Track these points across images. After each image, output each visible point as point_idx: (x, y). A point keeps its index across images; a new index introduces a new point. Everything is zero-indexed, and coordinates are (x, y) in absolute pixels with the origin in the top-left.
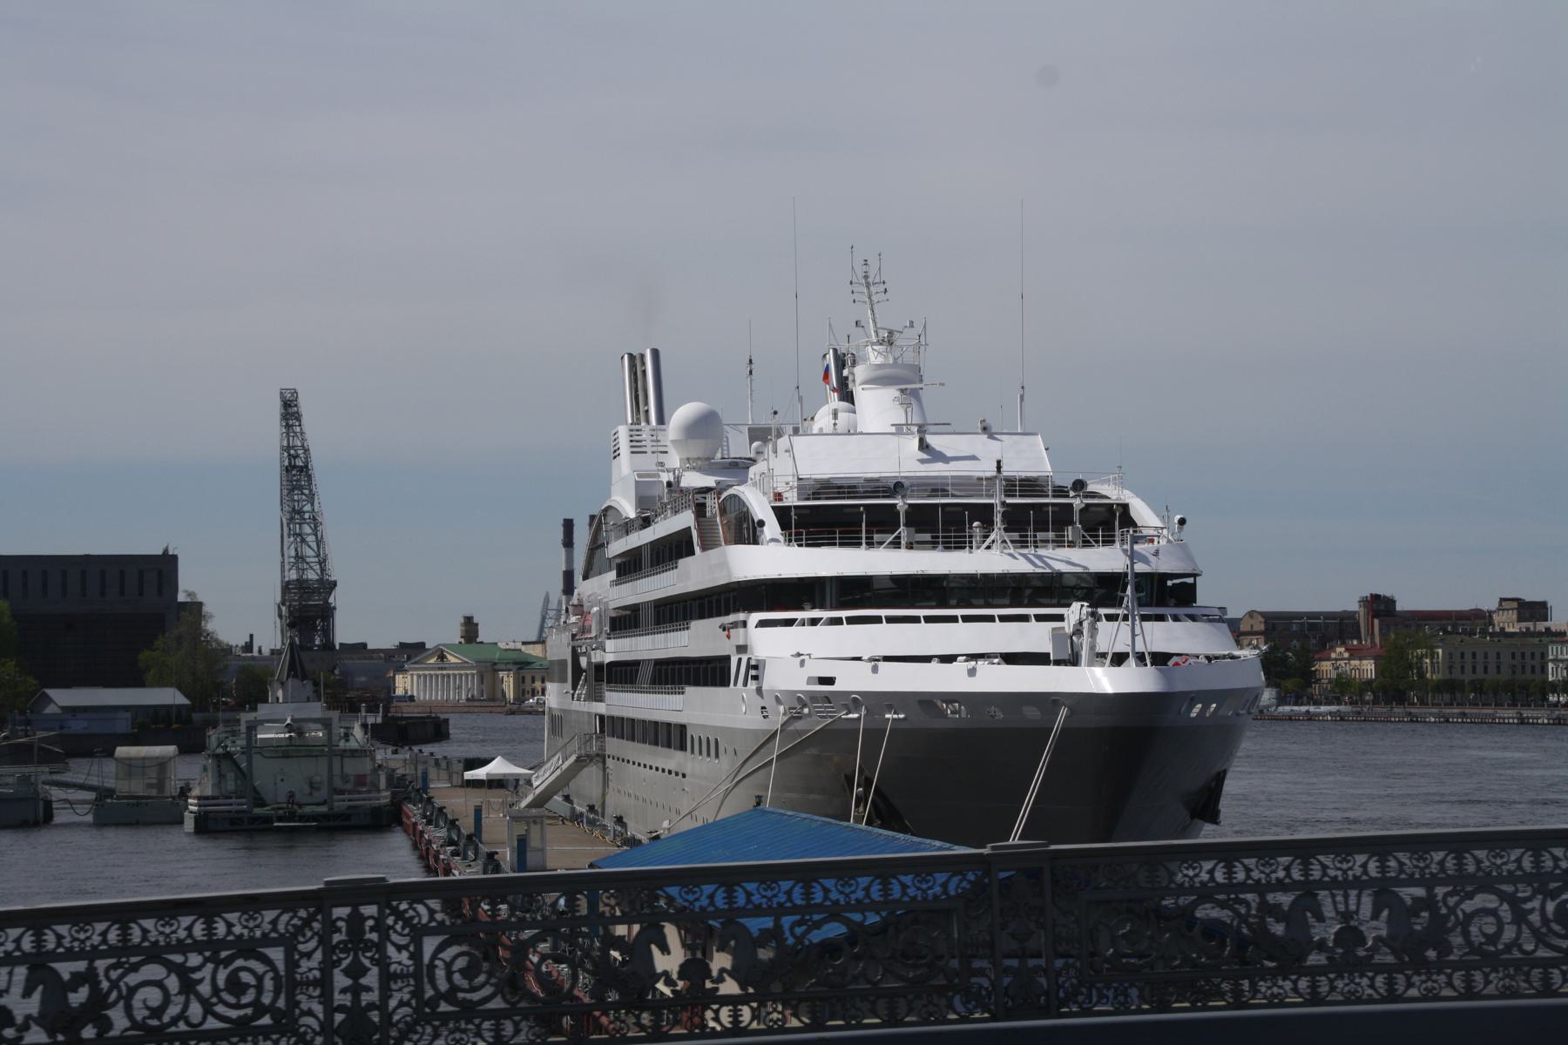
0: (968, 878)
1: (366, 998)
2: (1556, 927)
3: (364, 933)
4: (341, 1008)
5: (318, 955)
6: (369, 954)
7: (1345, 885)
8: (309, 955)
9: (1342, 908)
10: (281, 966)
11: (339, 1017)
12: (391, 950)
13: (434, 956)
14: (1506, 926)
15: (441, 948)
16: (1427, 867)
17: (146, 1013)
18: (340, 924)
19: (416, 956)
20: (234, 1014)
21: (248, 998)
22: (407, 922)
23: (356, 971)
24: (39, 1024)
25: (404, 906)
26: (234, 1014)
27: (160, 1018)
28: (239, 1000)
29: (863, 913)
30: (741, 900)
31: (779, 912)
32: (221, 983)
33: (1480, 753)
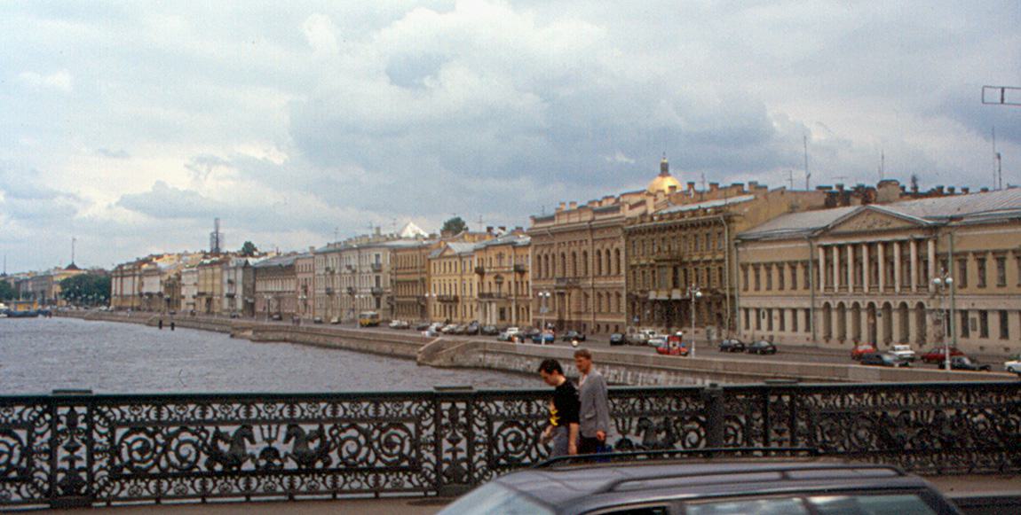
1: (78, 464)
3: (458, 418)
4: (447, 461)
5: (432, 428)
7: (269, 422)
8: (427, 428)
9: (266, 435)
10: (25, 442)
11: (60, 476)
12: (95, 436)
13: (122, 440)
15: (126, 435)
16: (359, 411)
19: (111, 440)
20: (389, 459)
21: (397, 449)
22: (107, 420)
23: (72, 448)
24: (293, 459)
25: (483, 404)
26: (389, 459)
30: (254, 414)
31: (319, 421)
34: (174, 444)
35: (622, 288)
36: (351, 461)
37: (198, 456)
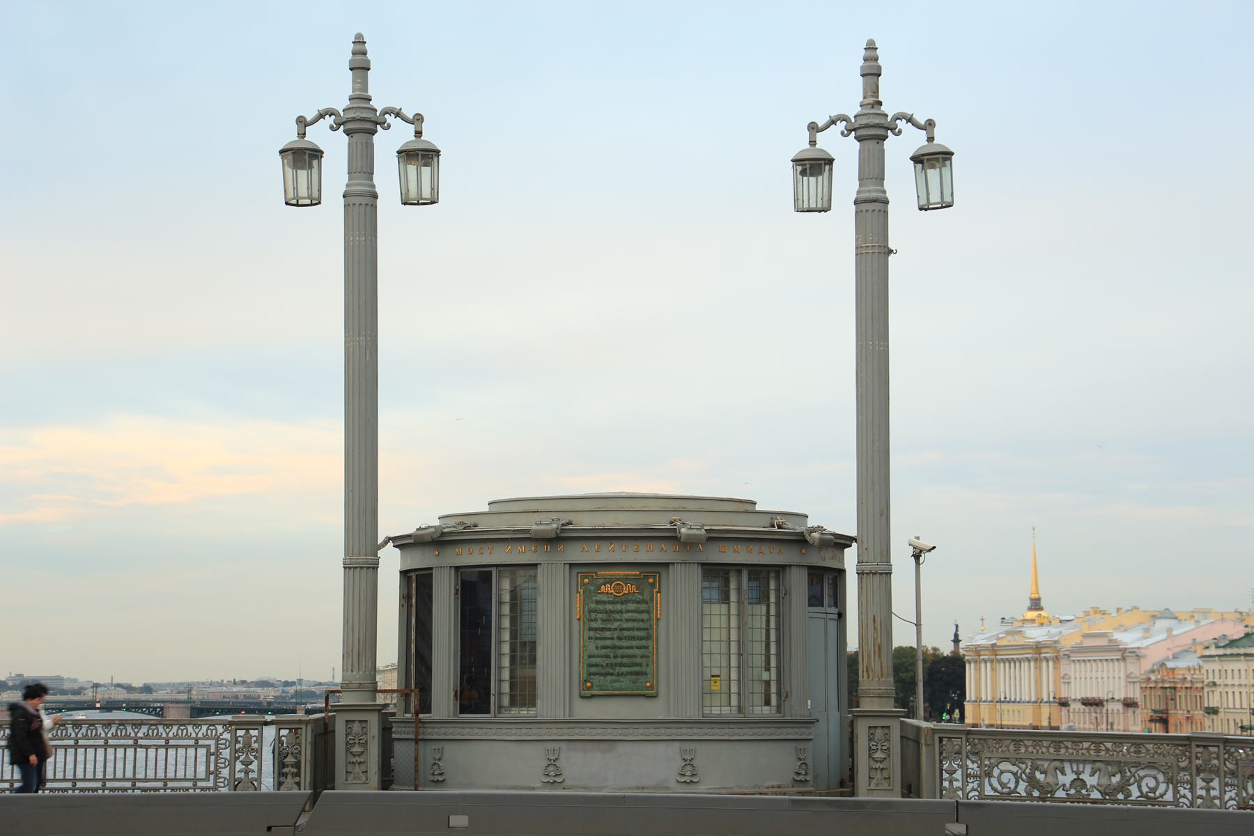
4: (1200, 797)
6: (957, 763)
14: (1161, 784)
17: (1148, 790)
18: (240, 739)
27: (1154, 793)
33: (633, 633)
34: (996, 772)
35: (842, 542)
36: (1152, 795)
37: (1017, 783)
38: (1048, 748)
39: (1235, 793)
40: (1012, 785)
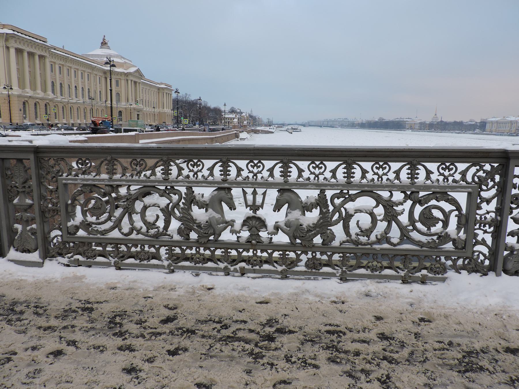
0: (485, 168)
2: (419, 225)
10: (464, 206)
17: (358, 231)
26: (424, 239)
28: (429, 229)
29: (390, 192)
32: (417, 216)
34: (138, 206)
36: (363, 239)
38: (153, 169)
39: (480, 208)
40: (161, 224)
